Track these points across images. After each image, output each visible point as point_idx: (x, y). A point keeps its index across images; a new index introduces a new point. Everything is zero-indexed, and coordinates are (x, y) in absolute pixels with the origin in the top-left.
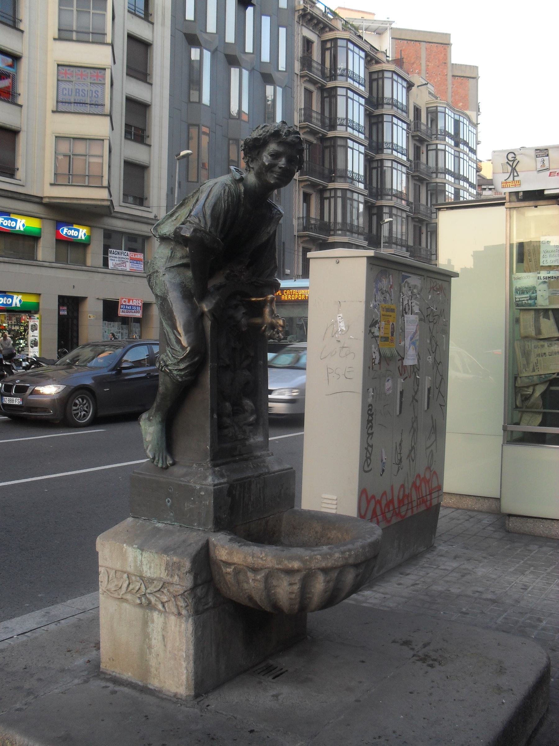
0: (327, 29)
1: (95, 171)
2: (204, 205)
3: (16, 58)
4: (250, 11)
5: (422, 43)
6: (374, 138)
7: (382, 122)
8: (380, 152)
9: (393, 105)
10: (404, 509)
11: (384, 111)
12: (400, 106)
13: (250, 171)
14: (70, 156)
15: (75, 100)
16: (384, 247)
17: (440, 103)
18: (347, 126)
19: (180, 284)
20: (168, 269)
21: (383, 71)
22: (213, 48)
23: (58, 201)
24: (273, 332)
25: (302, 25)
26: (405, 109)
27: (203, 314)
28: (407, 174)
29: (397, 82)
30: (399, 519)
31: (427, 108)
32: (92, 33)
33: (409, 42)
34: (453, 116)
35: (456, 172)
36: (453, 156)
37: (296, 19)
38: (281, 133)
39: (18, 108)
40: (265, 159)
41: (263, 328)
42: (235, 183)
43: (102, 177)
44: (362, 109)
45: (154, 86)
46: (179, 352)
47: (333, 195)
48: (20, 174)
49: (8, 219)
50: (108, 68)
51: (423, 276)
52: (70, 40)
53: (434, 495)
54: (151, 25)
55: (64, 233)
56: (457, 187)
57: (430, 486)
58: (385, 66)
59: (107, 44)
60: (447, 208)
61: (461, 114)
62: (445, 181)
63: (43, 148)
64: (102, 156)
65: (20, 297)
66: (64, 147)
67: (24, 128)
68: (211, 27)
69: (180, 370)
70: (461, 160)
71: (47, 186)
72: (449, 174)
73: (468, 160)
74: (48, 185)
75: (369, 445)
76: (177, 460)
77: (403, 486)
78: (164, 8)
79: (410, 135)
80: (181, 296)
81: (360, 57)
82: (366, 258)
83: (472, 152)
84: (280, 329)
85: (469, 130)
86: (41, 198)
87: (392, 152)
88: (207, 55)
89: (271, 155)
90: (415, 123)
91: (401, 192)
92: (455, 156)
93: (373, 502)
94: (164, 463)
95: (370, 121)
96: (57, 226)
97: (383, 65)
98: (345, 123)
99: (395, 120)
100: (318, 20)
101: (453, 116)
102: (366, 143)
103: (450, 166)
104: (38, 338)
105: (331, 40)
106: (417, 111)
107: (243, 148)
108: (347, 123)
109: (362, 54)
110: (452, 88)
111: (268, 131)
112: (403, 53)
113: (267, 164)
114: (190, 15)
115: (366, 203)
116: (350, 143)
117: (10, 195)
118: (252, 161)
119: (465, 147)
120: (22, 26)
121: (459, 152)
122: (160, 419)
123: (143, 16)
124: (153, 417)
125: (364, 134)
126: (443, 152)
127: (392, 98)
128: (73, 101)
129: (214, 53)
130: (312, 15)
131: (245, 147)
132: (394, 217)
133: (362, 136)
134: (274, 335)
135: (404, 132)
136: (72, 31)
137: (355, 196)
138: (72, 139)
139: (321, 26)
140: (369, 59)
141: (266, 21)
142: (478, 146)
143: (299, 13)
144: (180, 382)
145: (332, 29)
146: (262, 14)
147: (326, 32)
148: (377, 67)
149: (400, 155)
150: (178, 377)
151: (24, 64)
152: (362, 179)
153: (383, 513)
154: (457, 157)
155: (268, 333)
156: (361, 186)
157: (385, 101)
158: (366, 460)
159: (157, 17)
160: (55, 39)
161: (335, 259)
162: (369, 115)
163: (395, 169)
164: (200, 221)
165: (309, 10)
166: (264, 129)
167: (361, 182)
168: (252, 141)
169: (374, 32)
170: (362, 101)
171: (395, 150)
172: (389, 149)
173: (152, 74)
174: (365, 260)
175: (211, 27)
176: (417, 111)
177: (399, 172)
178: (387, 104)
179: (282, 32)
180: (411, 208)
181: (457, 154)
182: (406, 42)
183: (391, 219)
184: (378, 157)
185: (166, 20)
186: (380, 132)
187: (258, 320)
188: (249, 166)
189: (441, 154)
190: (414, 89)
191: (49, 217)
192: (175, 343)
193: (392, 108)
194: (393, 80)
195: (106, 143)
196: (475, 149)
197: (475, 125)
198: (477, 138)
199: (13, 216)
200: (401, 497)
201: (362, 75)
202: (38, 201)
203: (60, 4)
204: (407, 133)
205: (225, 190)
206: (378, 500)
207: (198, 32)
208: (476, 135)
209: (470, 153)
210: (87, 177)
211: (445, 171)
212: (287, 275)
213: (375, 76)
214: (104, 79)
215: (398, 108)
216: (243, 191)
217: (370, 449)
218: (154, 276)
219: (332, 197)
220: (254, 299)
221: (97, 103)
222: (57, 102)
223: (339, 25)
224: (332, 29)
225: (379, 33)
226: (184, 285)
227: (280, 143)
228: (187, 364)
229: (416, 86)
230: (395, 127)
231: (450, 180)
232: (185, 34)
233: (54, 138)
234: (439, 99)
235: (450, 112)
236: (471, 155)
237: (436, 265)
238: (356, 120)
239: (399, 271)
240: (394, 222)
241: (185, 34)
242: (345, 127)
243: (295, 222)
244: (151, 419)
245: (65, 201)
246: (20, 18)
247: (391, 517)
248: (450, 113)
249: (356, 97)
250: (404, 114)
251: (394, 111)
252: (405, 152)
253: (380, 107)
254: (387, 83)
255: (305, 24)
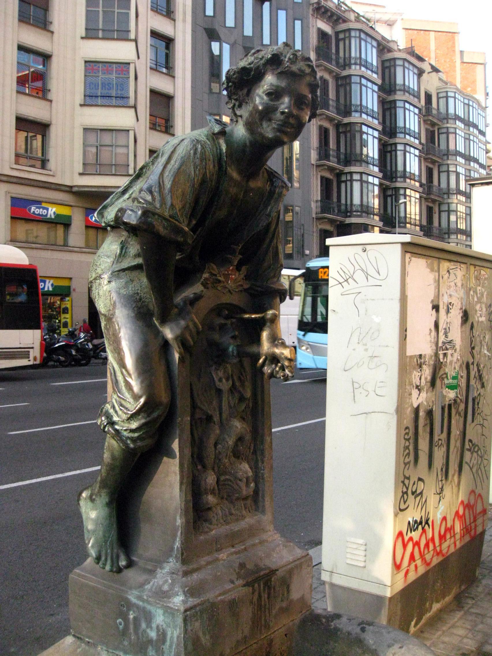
0: (341, 21)
1: (121, 160)
2: (162, 174)
3: (46, 57)
4: (267, 5)
5: (431, 32)
6: (388, 123)
7: (395, 108)
8: (392, 136)
9: (404, 91)
10: (445, 545)
11: (397, 97)
12: (411, 91)
13: (237, 121)
14: (97, 147)
15: (101, 93)
16: (399, 227)
17: (450, 88)
18: (361, 112)
19: (132, 296)
20: (116, 273)
21: (394, 59)
22: (232, 40)
23: (86, 189)
24: (275, 368)
25: (317, 18)
26: (416, 94)
27: (166, 345)
28: (420, 157)
29: (409, 69)
30: (440, 558)
31: (438, 94)
32: (117, 31)
33: (419, 31)
34: (462, 100)
35: (467, 153)
36: (463, 139)
37: (311, 12)
38: (282, 58)
39: (48, 103)
40: (258, 100)
41: (261, 361)
42: (213, 138)
43: (128, 165)
44: (375, 96)
45: (176, 78)
46: (130, 403)
47: (349, 178)
48: (52, 165)
49: (39, 208)
50: (132, 63)
51: (466, 263)
52: (97, 38)
53: (479, 521)
54: (173, 22)
55: (32, 212)
56: (468, 167)
57: (474, 511)
58: (397, 55)
59: (131, 40)
60: (482, 184)
61: (470, 98)
62: (456, 163)
63: (72, 140)
64: (127, 147)
65: (52, 281)
66: (92, 138)
67: (54, 122)
68: (230, 22)
69: (132, 431)
70: (472, 143)
71: (76, 176)
72: (460, 156)
73: (478, 142)
74: (77, 175)
75: (405, 477)
76: (134, 558)
77: (444, 519)
78: (184, 5)
79: (422, 120)
80: (133, 315)
81: (373, 46)
82: (399, 245)
83: (481, 134)
84: (286, 363)
85: (478, 114)
86: (71, 187)
87: (405, 136)
88: (226, 47)
89: (269, 94)
90: (426, 108)
91: (414, 174)
92: (465, 139)
93: (410, 546)
94: (115, 565)
95: (383, 106)
96: (86, 213)
97: (395, 53)
98: (359, 108)
99: (407, 106)
100: (332, 12)
101: (462, 100)
102: (380, 128)
103: (461, 148)
104: (68, 320)
105: (344, 31)
106: (428, 97)
107: (225, 86)
108: (362, 109)
109: (375, 43)
110: (461, 74)
111: (263, 57)
112: (413, 43)
113: (260, 108)
114: (210, 12)
115: (381, 185)
116: (364, 129)
117: (41, 185)
118: (240, 106)
119: (475, 130)
120: (52, 28)
121: (469, 135)
122: (107, 500)
123: (165, 13)
124: (96, 495)
125: (378, 119)
126: (454, 135)
127: (404, 84)
128: (99, 94)
129: (233, 47)
130: (325, 8)
131: (228, 83)
132: (407, 198)
133: (376, 122)
134: (277, 372)
135: (416, 117)
136: (98, 30)
137: (370, 179)
138: (99, 131)
139: (335, 18)
140: (381, 47)
141: (282, 15)
142: (487, 128)
143: (313, 6)
144: (132, 449)
145: (345, 21)
146: (278, 9)
147: (340, 23)
148: (389, 56)
149: (412, 139)
150: (129, 442)
151: (55, 62)
152: (376, 162)
153: (422, 556)
154: (467, 139)
155: (267, 370)
156: (376, 169)
157: (397, 88)
158: (403, 496)
159: (179, 15)
160: (82, 38)
161: (361, 247)
162: (382, 102)
163: (408, 152)
164: (154, 199)
165: (322, 4)
166: (256, 55)
167: (376, 166)
168: (238, 72)
169: (385, 23)
170: (376, 88)
171: (408, 134)
172: (402, 133)
173: (175, 67)
174: (399, 247)
175: (230, 22)
176: (428, 97)
177: (412, 156)
178: (400, 90)
179: (298, 24)
180: (424, 189)
181: (467, 136)
182: (416, 32)
183: (405, 200)
184: (392, 141)
185: (187, 16)
186: (394, 117)
187: (254, 349)
188: (235, 114)
189: (451, 137)
190: (425, 76)
191: (77, 205)
192: (124, 388)
193: (404, 94)
194: (404, 67)
195: (131, 134)
196: (484, 131)
197: (484, 109)
198: (486, 121)
199: (44, 205)
200: (442, 533)
201: (375, 63)
202: (69, 190)
203: (87, 6)
204: (419, 118)
205: (196, 149)
206: (417, 541)
207: (217, 27)
208: (485, 117)
209: (480, 135)
210: (114, 167)
211: (456, 152)
212: (307, 255)
213: (387, 64)
214: (129, 73)
215: (410, 94)
216: (224, 151)
217: (406, 482)
218: (97, 284)
219: (349, 180)
220: (247, 316)
221: (122, 96)
222: (85, 96)
223: (352, 17)
224: (345, 21)
225: (390, 24)
226: (138, 297)
227: (281, 75)
228: (143, 421)
229: (426, 73)
230: (407, 112)
231: (461, 161)
232: (205, 29)
233: (82, 130)
234: (449, 84)
235: (459, 96)
236: (481, 137)
237: (470, 246)
238: (370, 106)
239: (439, 258)
240: (408, 203)
241: (205, 29)
242: (359, 113)
243: (313, 205)
244: (94, 499)
245: (93, 190)
246: (50, 20)
247: (432, 559)
248: (460, 97)
249: (369, 84)
250: (416, 100)
251: (407, 97)
252: (417, 136)
253: (393, 93)
254: (399, 71)
255: (319, 17)
